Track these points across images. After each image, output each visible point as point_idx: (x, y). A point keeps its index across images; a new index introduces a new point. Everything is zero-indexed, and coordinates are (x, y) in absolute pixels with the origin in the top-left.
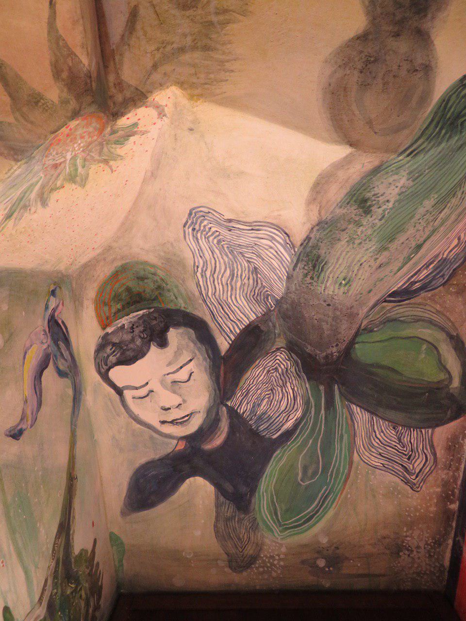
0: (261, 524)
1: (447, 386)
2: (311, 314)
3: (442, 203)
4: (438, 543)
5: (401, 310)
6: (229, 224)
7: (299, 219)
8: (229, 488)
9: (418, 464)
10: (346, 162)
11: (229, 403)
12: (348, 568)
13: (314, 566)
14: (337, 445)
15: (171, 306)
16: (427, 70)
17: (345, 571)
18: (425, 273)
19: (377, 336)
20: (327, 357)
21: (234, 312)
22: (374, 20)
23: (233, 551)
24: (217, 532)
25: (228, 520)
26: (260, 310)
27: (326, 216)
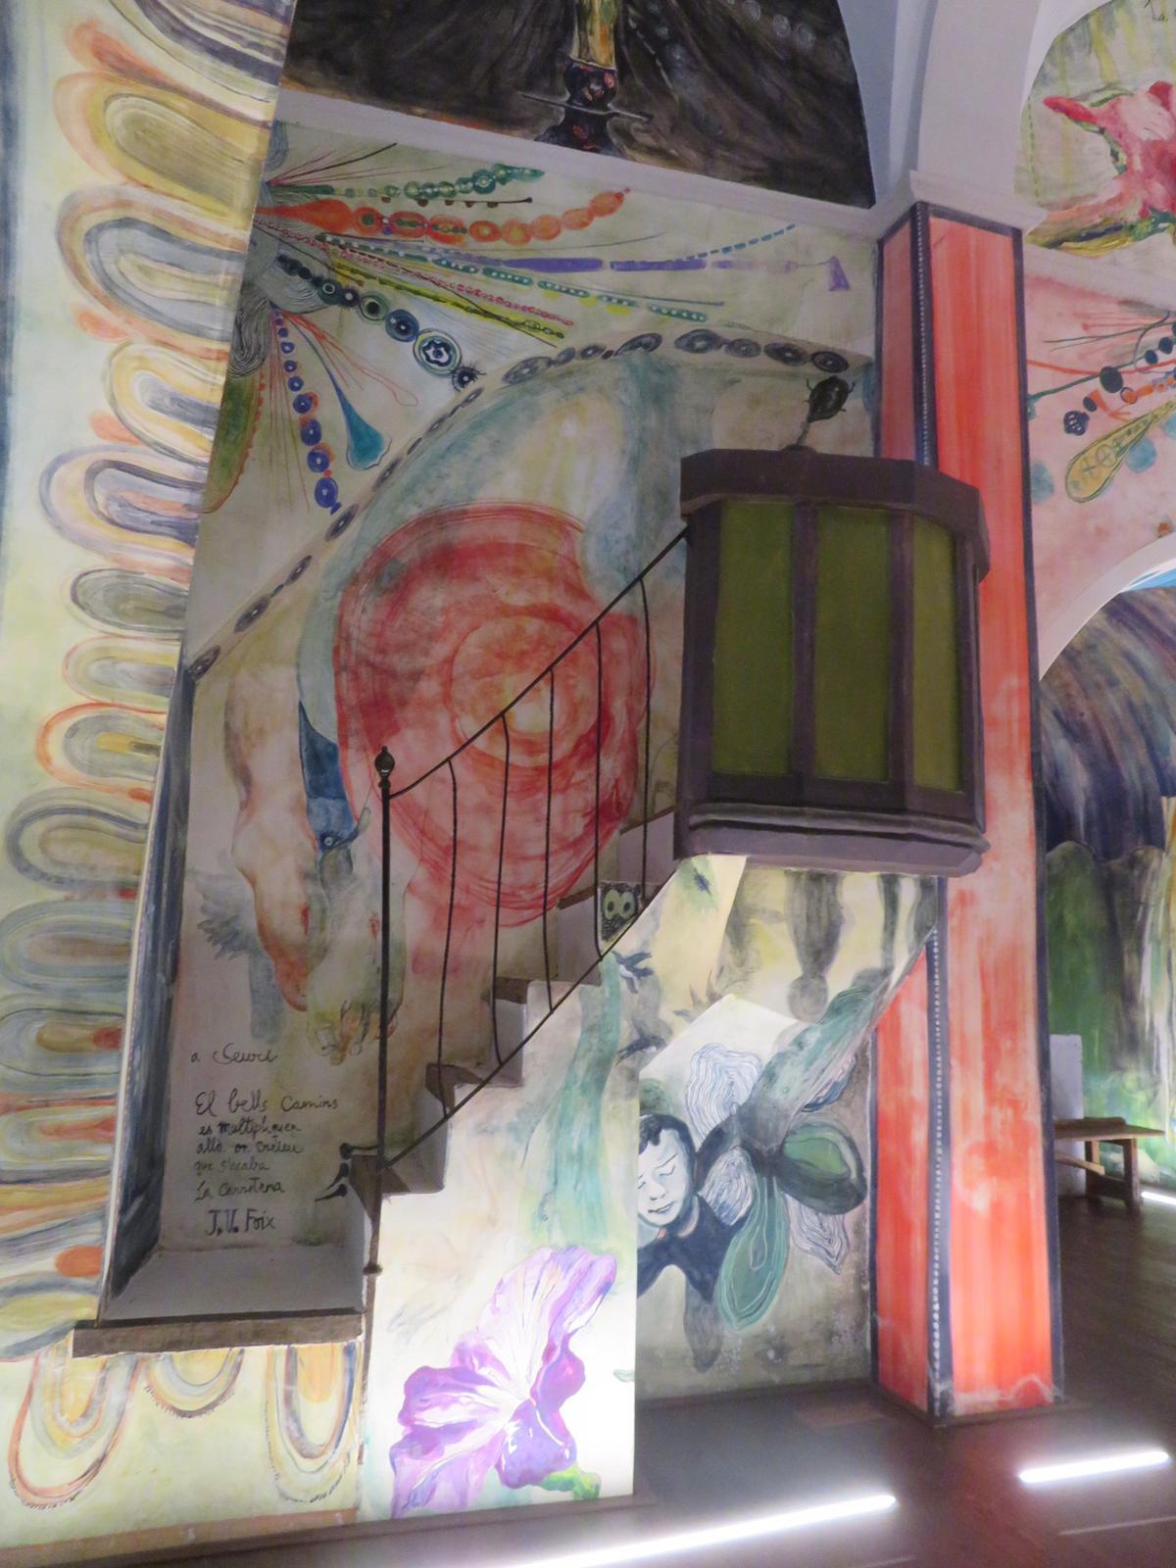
0: (722, 1316)
1: (848, 1178)
2: (762, 1115)
3: (834, 1045)
4: (860, 1325)
5: (812, 1118)
6: (727, 1054)
7: (768, 1053)
8: (696, 1274)
9: (835, 1248)
10: (796, 1025)
11: (700, 1193)
12: (797, 1358)
13: (766, 1359)
14: (777, 1232)
15: (664, 1113)
16: (825, 991)
17: (791, 1362)
18: (825, 1091)
19: (800, 1137)
20: (769, 1152)
21: (705, 1117)
22: (805, 970)
23: (698, 1346)
24: (686, 1324)
25: (697, 1309)
26: (725, 1115)
27: (782, 1050)
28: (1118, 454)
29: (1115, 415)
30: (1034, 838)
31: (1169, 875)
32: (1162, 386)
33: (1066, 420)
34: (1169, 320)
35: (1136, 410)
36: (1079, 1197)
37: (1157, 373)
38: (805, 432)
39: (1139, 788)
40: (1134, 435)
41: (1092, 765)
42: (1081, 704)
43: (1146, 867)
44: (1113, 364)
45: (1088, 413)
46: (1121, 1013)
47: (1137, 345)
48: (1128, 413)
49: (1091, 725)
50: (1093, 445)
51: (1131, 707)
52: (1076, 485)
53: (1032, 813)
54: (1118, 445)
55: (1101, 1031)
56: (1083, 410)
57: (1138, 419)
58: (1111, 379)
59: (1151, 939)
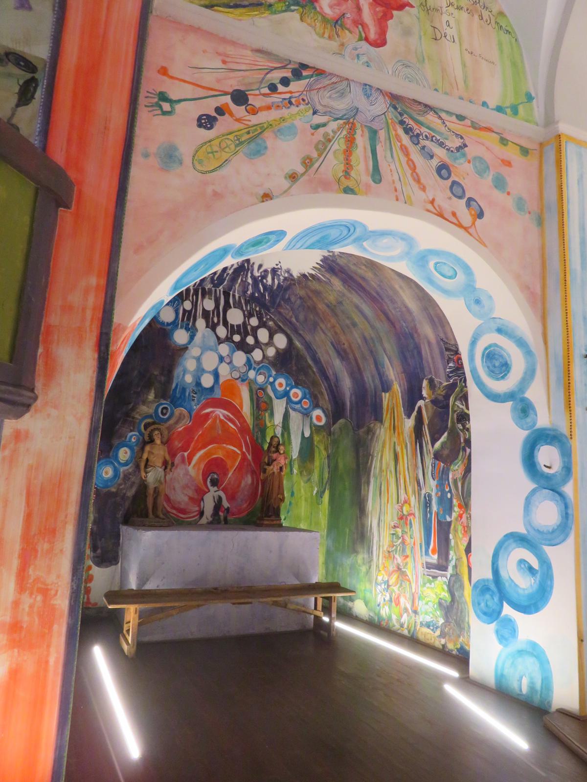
28: (236, 146)
29: (238, 120)
30: (93, 394)
31: (383, 438)
32: (278, 106)
33: (199, 119)
34: (289, 66)
35: (254, 120)
36: (309, 631)
37: (276, 98)
38: (13, 115)
39: (373, 387)
40: (251, 135)
41: (352, 375)
42: (343, 338)
43: (374, 434)
44: (242, 88)
45: (218, 116)
46: (359, 519)
47: (263, 79)
48: (250, 121)
49: (348, 350)
50: (218, 137)
51: (365, 339)
52: (200, 162)
53: (95, 375)
54: (238, 139)
55: (350, 530)
56: (214, 114)
57: (256, 125)
58: (240, 97)
59: (374, 476)
